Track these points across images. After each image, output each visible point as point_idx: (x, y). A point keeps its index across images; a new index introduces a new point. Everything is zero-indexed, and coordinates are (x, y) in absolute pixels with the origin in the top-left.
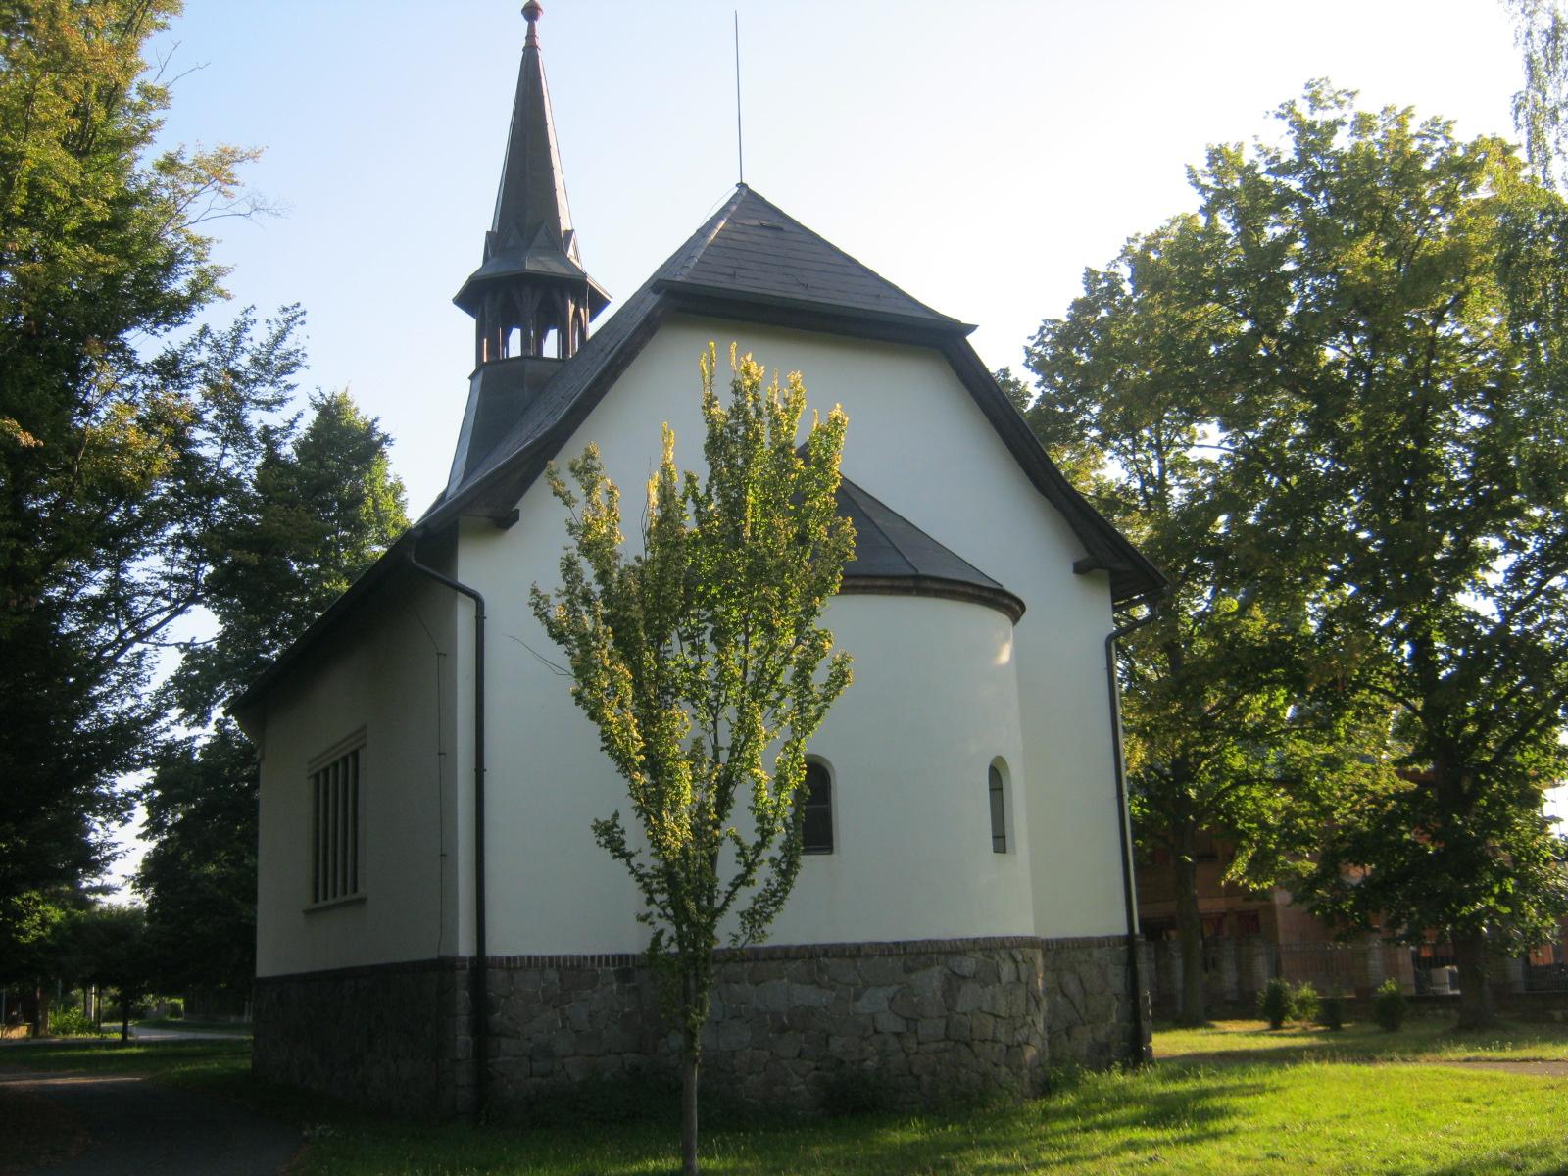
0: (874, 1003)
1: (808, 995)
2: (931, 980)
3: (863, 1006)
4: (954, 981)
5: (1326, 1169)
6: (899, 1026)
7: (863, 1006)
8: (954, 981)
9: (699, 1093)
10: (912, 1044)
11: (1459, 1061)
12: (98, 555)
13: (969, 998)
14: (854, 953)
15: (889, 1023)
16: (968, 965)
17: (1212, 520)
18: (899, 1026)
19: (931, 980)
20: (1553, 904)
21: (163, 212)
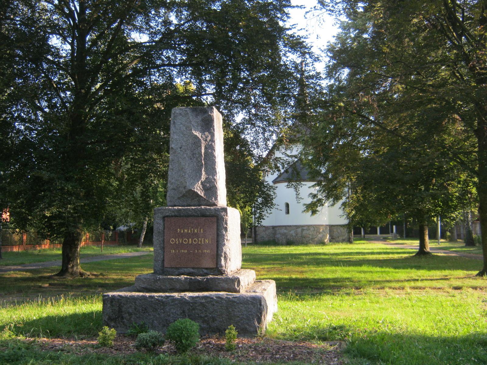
0: (292, 232)
1: (285, 231)
2: (299, 230)
3: (291, 232)
4: (303, 230)
5: (485, 289)
6: (295, 235)
7: (291, 232)
8: (303, 230)
9: (403, 232)
10: (297, 237)
11: (298, 271)
12: (157, 130)
13: (305, 232)
14: (290, 226)
15: (294, 235)
16: (305, 228)
17: (333, 176)
18: (295, 235)
19: (299, 230)
20: (481, 1)
21: (375, 339)
